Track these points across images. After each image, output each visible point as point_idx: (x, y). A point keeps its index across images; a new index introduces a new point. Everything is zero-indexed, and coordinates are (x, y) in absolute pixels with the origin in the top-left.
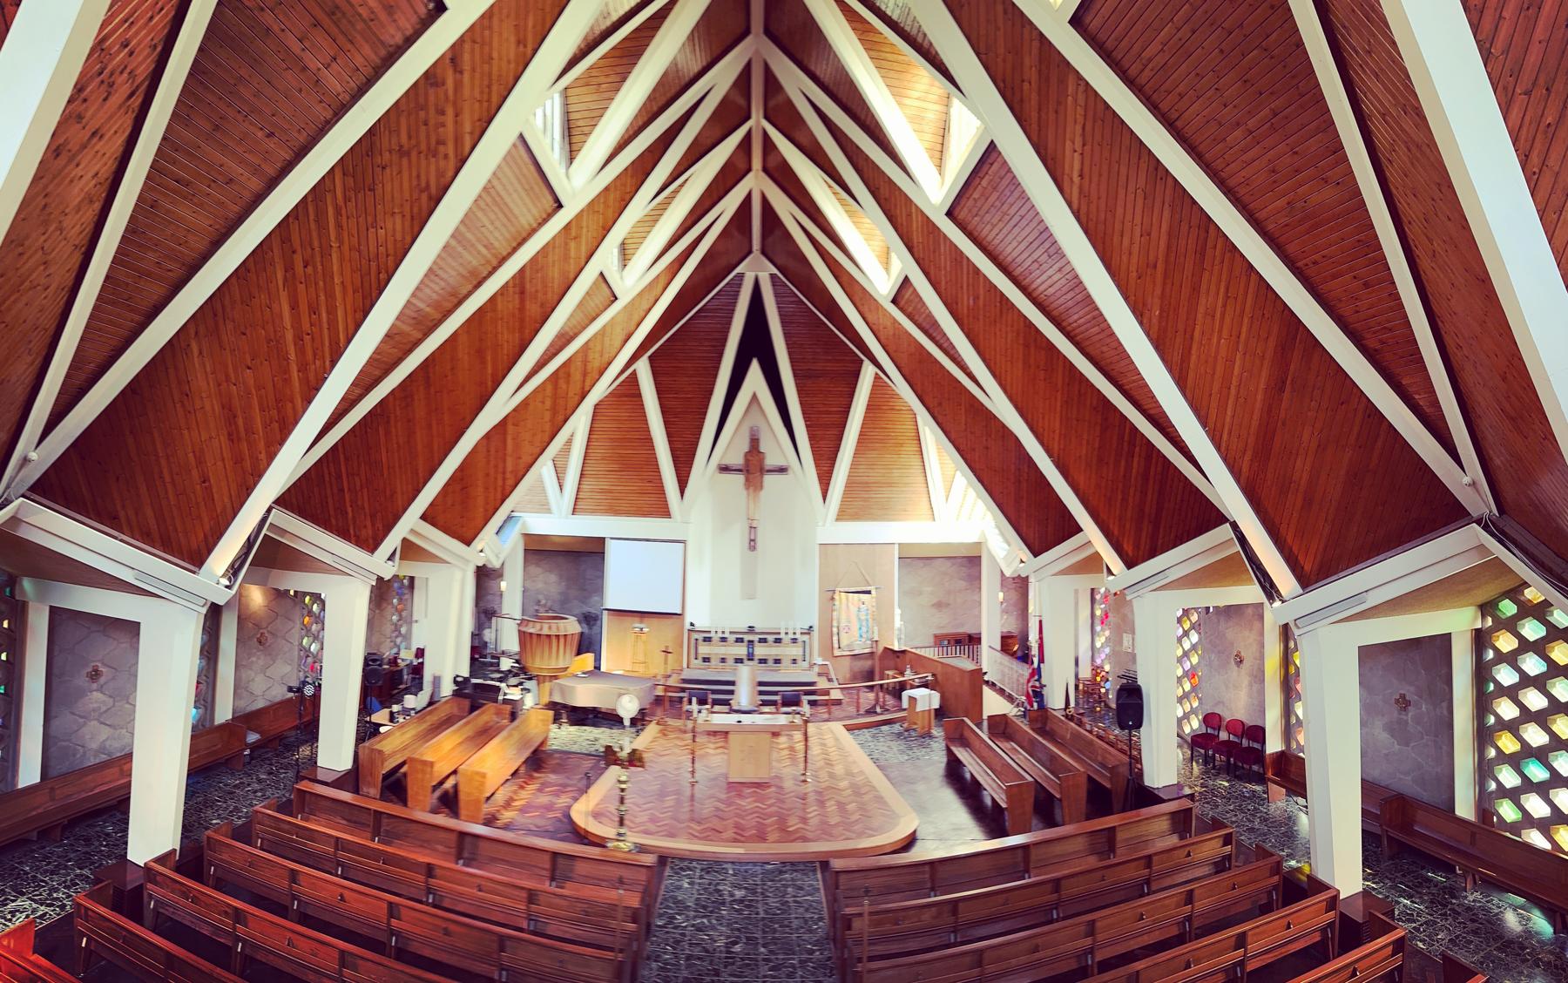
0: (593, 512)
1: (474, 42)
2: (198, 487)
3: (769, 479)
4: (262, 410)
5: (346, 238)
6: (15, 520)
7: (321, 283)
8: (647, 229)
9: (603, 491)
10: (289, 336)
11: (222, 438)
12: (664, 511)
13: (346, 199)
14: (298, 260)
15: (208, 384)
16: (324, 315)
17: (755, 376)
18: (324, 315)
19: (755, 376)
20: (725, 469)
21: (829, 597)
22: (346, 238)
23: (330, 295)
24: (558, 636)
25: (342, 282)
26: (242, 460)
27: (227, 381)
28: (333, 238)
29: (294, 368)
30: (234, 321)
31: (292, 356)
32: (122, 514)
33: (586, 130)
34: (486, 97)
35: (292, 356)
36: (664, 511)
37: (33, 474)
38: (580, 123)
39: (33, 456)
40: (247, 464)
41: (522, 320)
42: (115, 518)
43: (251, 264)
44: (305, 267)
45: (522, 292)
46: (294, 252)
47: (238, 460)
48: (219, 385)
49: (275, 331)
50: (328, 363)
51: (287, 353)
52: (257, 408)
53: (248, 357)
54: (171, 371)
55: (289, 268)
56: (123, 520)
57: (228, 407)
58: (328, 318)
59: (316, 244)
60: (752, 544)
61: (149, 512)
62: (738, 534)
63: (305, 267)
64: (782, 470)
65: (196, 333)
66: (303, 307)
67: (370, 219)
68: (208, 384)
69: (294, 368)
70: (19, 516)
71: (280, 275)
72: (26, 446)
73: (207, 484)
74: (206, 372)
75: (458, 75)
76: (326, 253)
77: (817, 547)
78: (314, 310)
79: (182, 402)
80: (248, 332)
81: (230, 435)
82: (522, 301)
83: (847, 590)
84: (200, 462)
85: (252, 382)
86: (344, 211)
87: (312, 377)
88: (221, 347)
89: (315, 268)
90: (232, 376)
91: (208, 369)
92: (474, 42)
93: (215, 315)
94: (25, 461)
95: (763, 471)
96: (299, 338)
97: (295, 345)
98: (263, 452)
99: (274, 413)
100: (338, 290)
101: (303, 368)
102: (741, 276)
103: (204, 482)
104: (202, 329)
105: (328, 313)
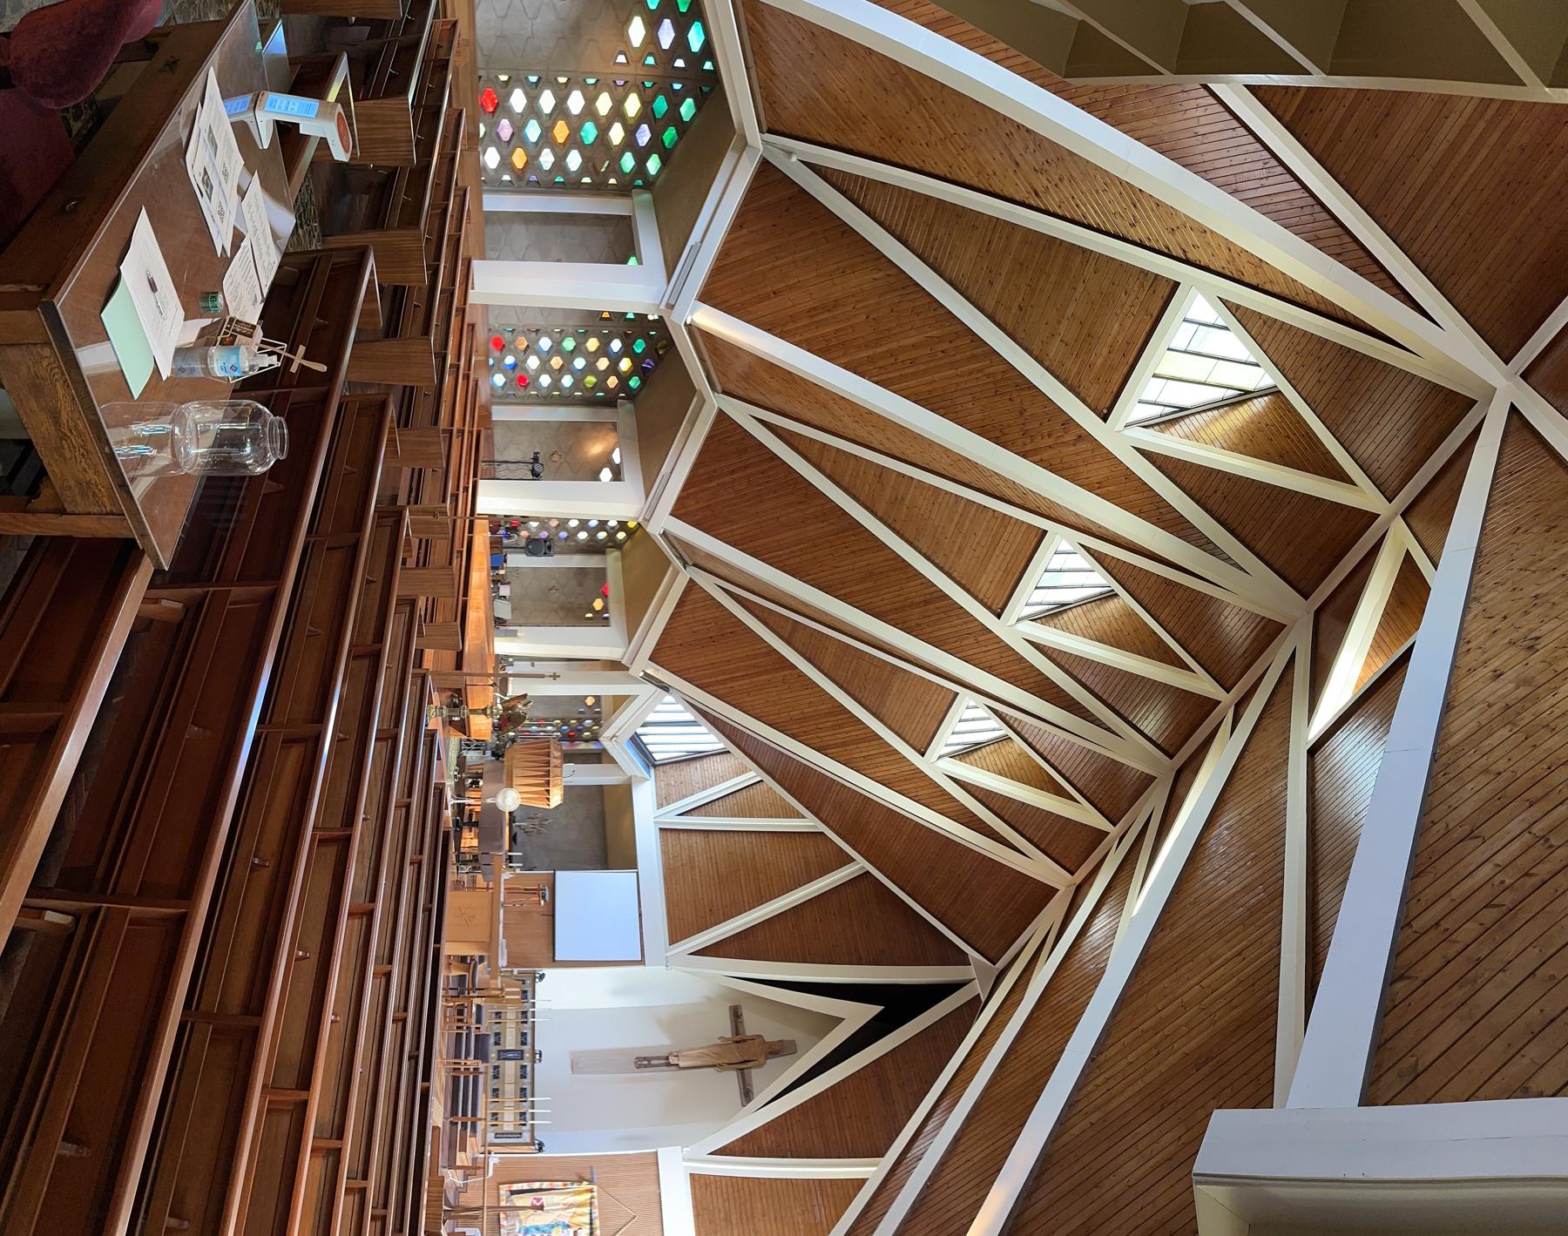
0: (664, 853)
1: (1093, 451)
2: (769, 289)
3: (732, 1077)
4: (836, 331)
5: (963, 379)
6: (744, 145)
7: (932, 365)
8: (991, 769)
9: (691, 860)
10: (893, 345)
11: (811, 302)
12: (677, 933)
13: (988, 376)
14: (945, 346)
15: (854, 287)
16: (910, 370)
17: (858, 1014)
18: (910, 370)
19: (858, 1014)
20: (736, 1014)
21: (581, 1174)
22: (963, 379)
23: (925, 372)
24: (548, 763)
25: (934, 381)
26: (794, 322)
27: (856, 301)
28: (963, 369)
29: (870, 352)
30: (900, 302)
31: (879, 350)
32: (744, 231)
33: (1058, 626)
34: (1065, 465)
35: (879, 350)
36: (677, 933)
37: (778, 161)
38: (1062, 621)
39: (794, 159)
40: (791, 326)
41: (903, 608)
42: (741, 227)
43: (942, 311)
44: (942, 352)
45: (926, 602)
46: (951, 342)
47: (793, 318)
48: (853, 296)
49: (895, 334)
50: (876, 379)
51: (881, 345)
52: (837, 328)
53: (875, 316)
54: (861, 259)
55: (940, 339)
56: (738, 233)
57: (836, 304)
58: (909, 374)
59: (958, 357)
60: (644, 1062)
61: (746, 253)
62: (656, 1040)
63: (942, 352)
64: (747, 1095)
65: (889, 275)
66: (913, 354)
67: (978, 395)
68: (854, 287)
69: (870, 352)
70: (747, 149)
71: (934, 333)
72: (804, 153)
73: (772, 296)
74: (861, 285)
75: (1072, 443)
76: (952, 365)
77: (654, 1150)
78: (913, 362)
79: (838, 269)
80: (893, 314)
81: (815, 308)
82: (918, 605)
83: (597, 1223)
84: (790, 288)
85: (857, 321)
86: (980, 375)
87: (864, 368)
88: (881, 294)
89: (941, 359)
90: (861, 305)
91: (864, 286)
92: (1093, 451)
93: (903, 288)
94: (789, 153)
95: (743, 1067)
96: (891, 353)
97: (887, 351)
98: (802, 338)
99: (834, 342)
100: (928, 378)
101: (871, 360)
102: (963, 960)
103: (774, 293)
104: (891, 279)
105: (912, 374)
